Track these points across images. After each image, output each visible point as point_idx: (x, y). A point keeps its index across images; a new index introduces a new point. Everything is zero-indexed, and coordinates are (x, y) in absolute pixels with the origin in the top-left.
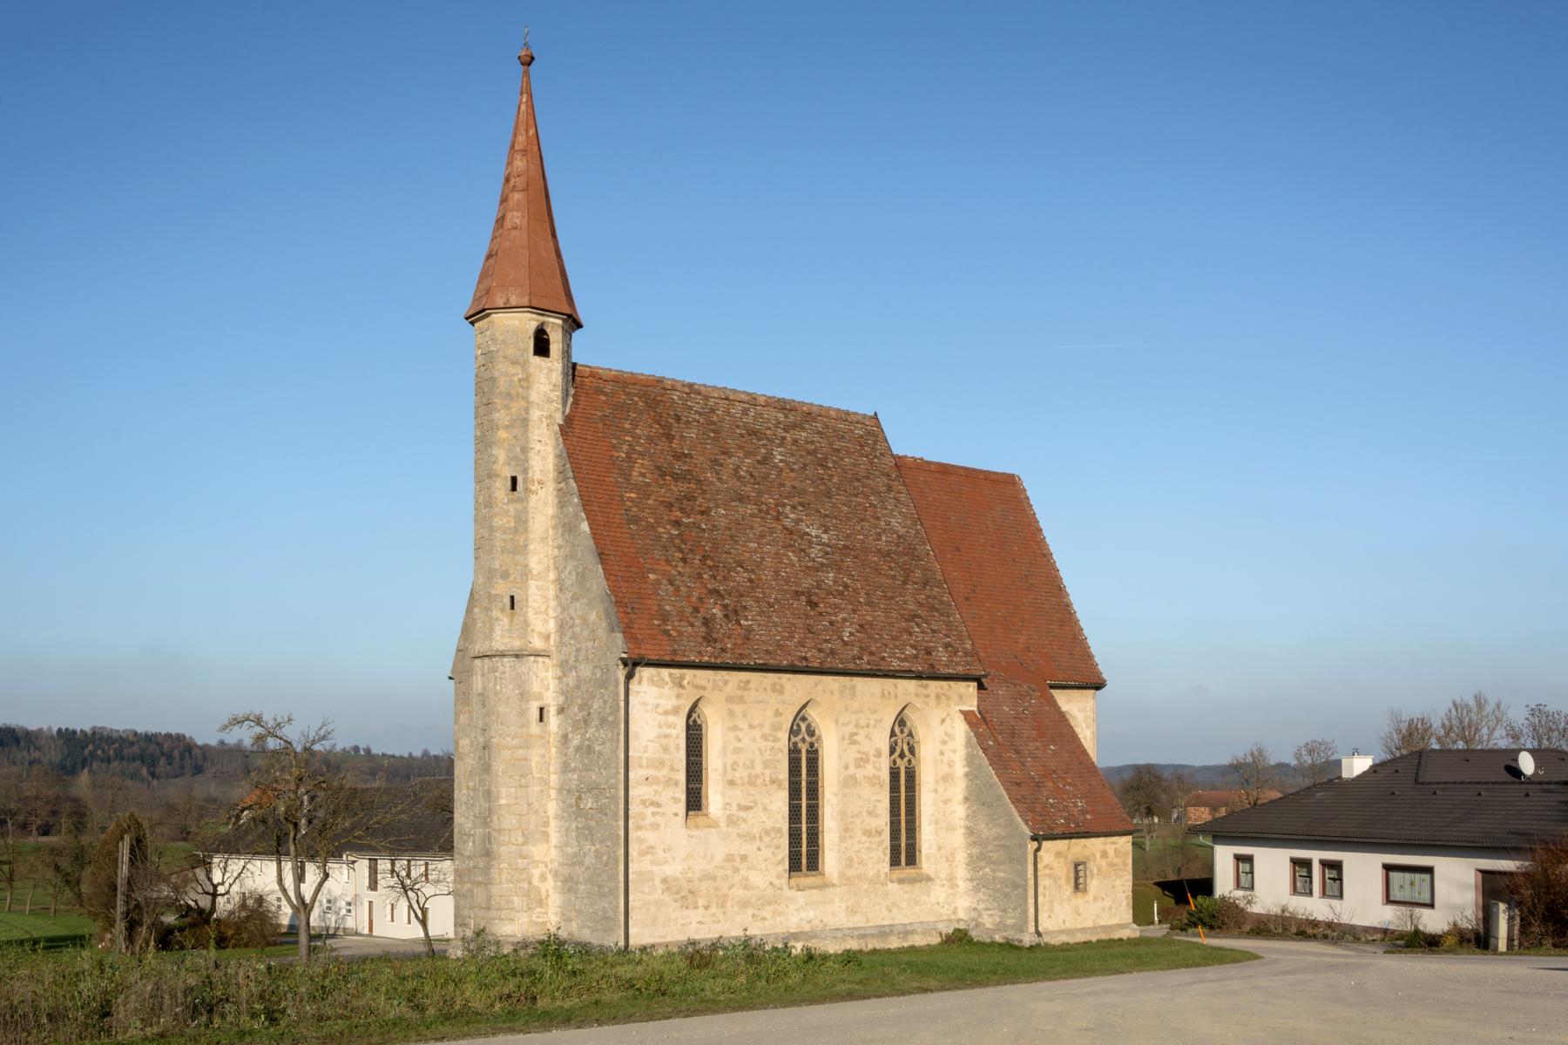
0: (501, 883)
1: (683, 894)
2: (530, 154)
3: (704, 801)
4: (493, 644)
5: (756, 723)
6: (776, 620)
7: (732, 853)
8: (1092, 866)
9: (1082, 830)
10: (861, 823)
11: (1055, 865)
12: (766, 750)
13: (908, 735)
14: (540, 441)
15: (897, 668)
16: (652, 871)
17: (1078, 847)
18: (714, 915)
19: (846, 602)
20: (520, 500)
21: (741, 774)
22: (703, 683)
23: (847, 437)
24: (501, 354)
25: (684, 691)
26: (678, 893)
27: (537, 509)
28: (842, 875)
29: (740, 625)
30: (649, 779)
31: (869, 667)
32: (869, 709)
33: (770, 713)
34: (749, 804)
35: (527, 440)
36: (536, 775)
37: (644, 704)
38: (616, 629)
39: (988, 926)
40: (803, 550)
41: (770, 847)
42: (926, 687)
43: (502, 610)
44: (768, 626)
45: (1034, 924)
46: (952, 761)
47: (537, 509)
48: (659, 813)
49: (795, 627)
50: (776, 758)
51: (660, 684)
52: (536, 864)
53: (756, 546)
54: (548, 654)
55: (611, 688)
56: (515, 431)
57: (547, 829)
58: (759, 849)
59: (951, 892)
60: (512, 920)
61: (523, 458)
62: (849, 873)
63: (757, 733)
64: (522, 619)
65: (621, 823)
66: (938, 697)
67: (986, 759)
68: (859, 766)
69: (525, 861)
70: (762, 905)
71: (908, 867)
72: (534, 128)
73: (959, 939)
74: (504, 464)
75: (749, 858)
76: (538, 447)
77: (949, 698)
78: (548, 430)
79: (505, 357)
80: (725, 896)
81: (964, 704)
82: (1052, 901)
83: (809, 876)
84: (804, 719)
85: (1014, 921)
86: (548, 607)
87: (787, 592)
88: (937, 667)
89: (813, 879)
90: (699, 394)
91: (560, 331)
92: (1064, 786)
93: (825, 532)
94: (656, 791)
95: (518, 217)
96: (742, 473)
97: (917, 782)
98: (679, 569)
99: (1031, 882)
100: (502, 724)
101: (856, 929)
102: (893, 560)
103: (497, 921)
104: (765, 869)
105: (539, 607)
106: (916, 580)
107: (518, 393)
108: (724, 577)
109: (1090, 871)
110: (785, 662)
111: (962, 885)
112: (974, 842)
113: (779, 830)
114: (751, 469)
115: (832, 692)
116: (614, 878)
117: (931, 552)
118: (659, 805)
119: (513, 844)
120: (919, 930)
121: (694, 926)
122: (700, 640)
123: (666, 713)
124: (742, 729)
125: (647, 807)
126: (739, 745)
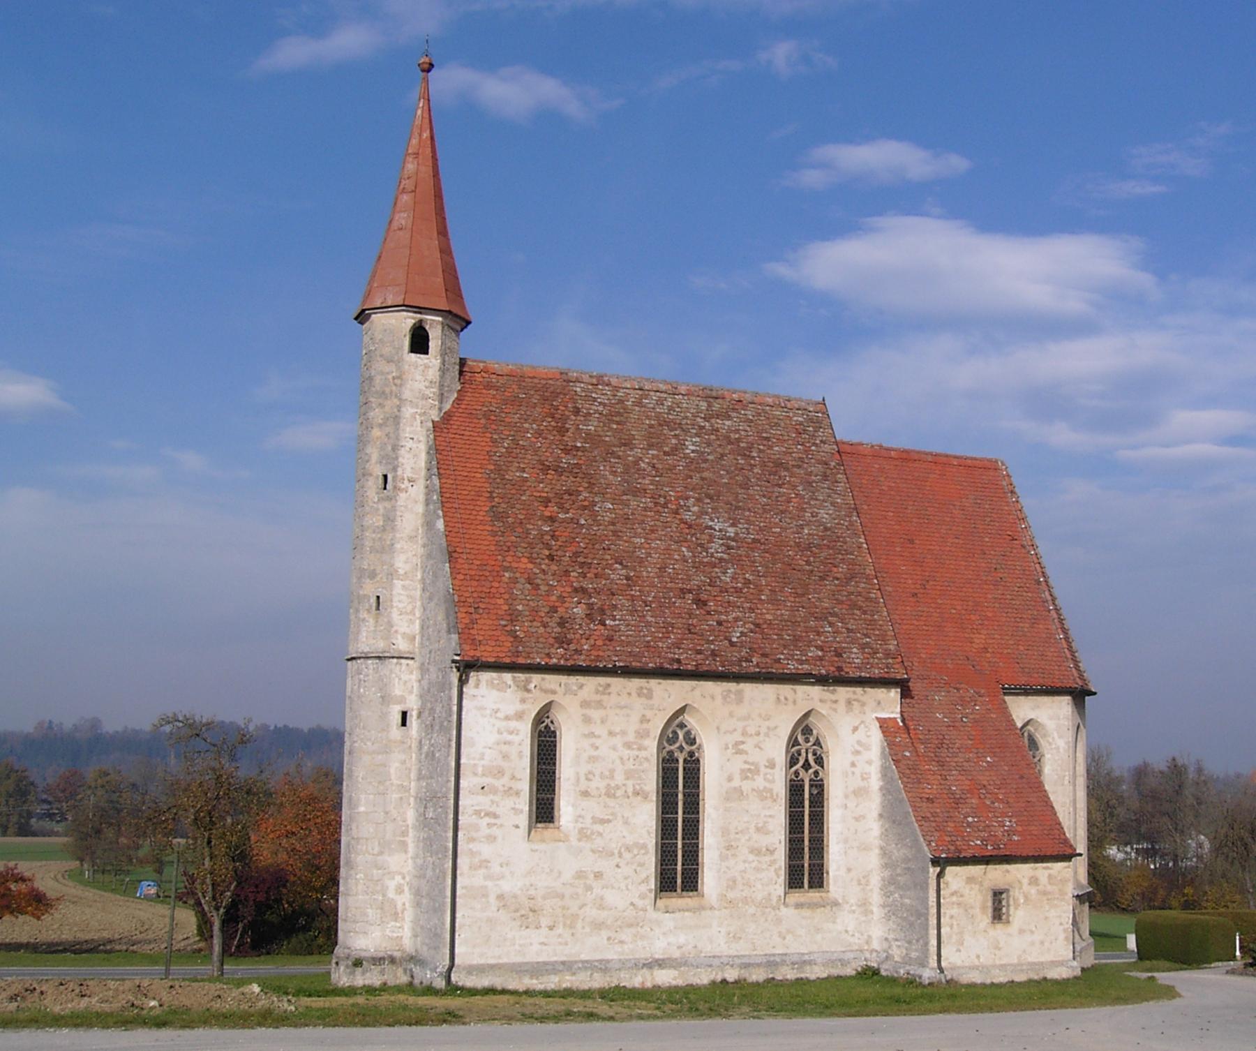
0: (357, 894)
1: (523, 912)
2: (421, 157)
3: (556, 813)
4: (359, 645)
5: (618, 730)
6: (650, 619)
7: (583, 869)
8: (1015, 893)
9: (1002, 852)
10: (749, 840)
11: (966, 891)
12: (629, 759)
13: (814, 745)
14: (412, 439)
15: (793, 671)
16: (486, 887)
17: (997, 874)
18: (560, 936)
19: (742, 599)
20: (389, 499)
21: (597, 784)
22: (553, 686)
23: (782, 425)
24: (378, 353)
25: (530, 695)
26: (517, 911)
27: (406, 507)
28: (722, 897)
29: (605, 625)
30: (485, 789)
31: (758, 670)
32: (760, 715)
33: (635, 718)
34: (607, 817)
35: (398, 439)
36: (395, 782)
37: (482, 708)
38: (452, 630)
39: (897, 959)
40: (701, 545)
41: (632, 864)
42: (833, 692)
43: (369, 611)
44: (639, 626)
45: (935, 958)
46: (866, 774)
47: (406, 507)
48: (495, 824)
49: (673, 627)
50: (641, 768)
51: (502, 687)
52: (392, 875)
53: (643, 540)
54: (411, 656)
55: (447, 692)
56: (387, 430)
57: (405, 839)
58: (618, 866)
59: (864, 919)
60: (365, 933)
61: (394, 456)
62: (731, 895)
63: (618, 741)
64: (386, 620)
65: (450, 834)
66: (849, 702)
67: (896, 771)
68: (747, 778)
69: (380, 871)
70: (620, 927)
71: (811, 890)
72: (428, 131)
73: (869, 974)
74: (376, 463)
75: (604, 876)
76: (410, 444)
77: (863, 704)
78: (421, 427)
79: (381, 356)
80: (576, 916)
81: (883, 710)
82: (961, 933)
83: (683, 897)
84: (682, 726)
85: (917, 954)
86: (414, 608)
87: (671, 589)
88: (846, 670)
89: (689, 900)
90: (607, 385)
91: (440, 327)
92: (993, 803)
93: (733, 525)
94: (493, 802)
95: (404, 218)
96: (643, 465)
97: (825, 797)
98: (543, 566)
99: (934, 911)
100: (364, 728)
101: (738, 957)
102: (814, 555)
103: (352, 934)
104: (624, 888)
105: (405, 608)
106: (838, 575)
107: (391, 392)
108: (595, 574)
109: (1014, 899)
110: (650, 665)
111: (878, 912)
112: (886, 864)
113: (644, 846)
114: (655, 461)
115: (713, 697)
116: (442, 891)
117: (865, 546)
118: (495, 816)
119: (369, 854)
120: (819, 961)
121: (536, 947)
122: (551, 641)
123: (507, 718)
124: (599, 737)
125: (482, 818)
126: (595, 753)
